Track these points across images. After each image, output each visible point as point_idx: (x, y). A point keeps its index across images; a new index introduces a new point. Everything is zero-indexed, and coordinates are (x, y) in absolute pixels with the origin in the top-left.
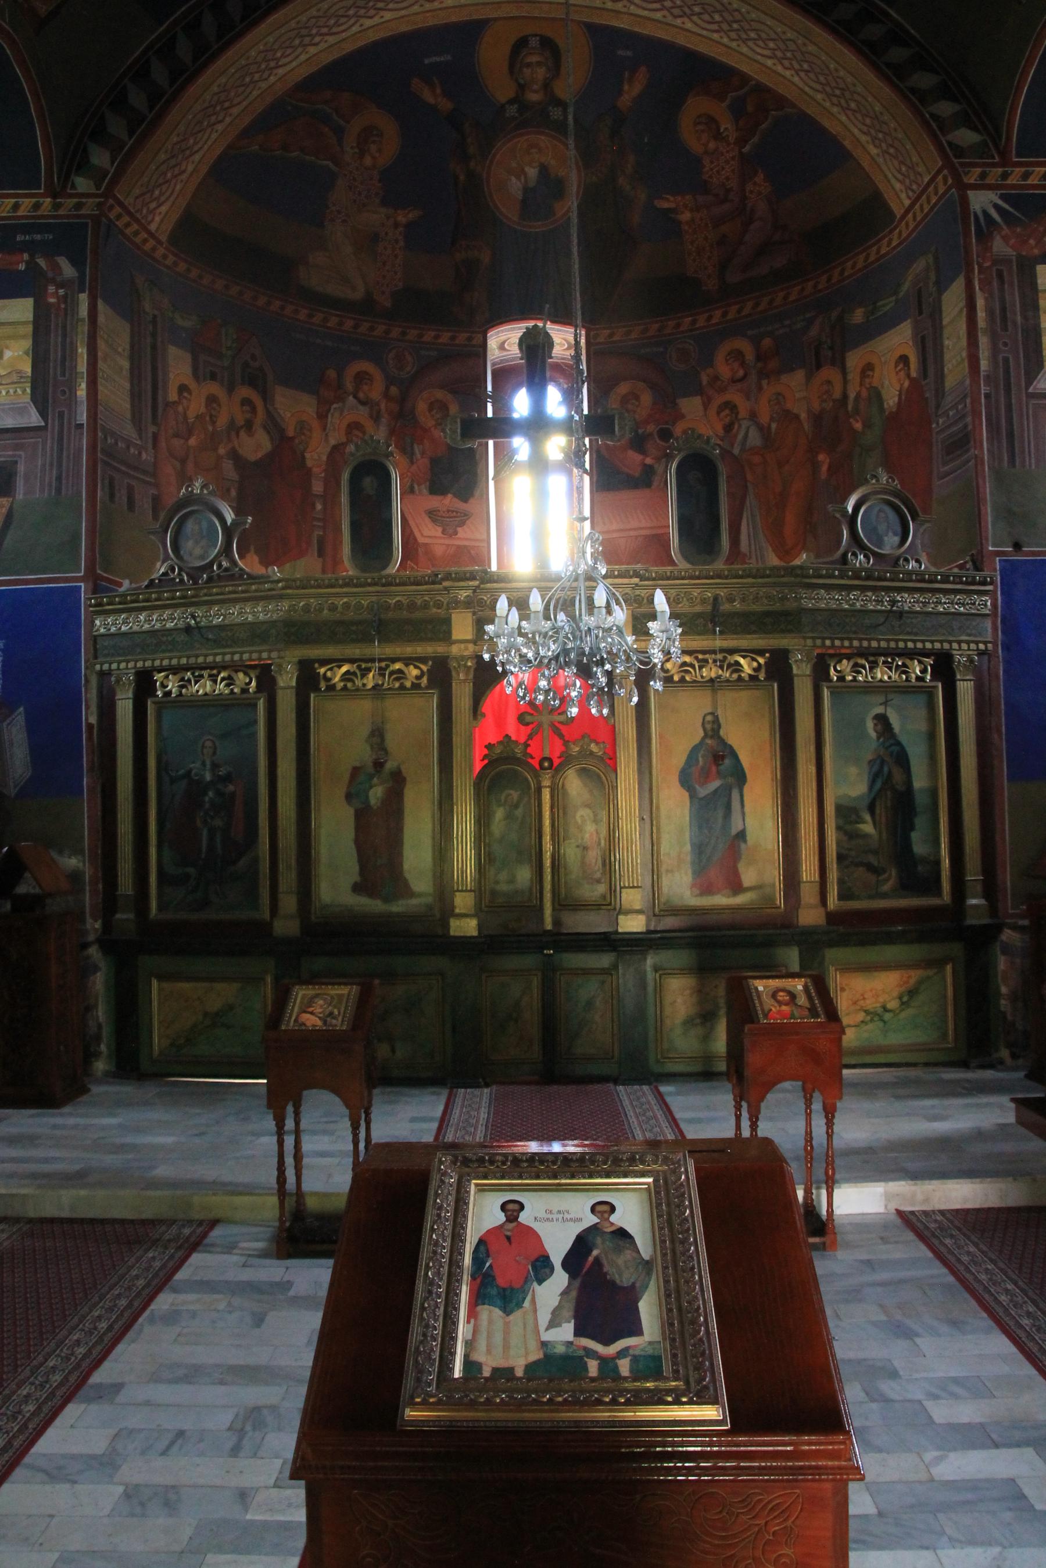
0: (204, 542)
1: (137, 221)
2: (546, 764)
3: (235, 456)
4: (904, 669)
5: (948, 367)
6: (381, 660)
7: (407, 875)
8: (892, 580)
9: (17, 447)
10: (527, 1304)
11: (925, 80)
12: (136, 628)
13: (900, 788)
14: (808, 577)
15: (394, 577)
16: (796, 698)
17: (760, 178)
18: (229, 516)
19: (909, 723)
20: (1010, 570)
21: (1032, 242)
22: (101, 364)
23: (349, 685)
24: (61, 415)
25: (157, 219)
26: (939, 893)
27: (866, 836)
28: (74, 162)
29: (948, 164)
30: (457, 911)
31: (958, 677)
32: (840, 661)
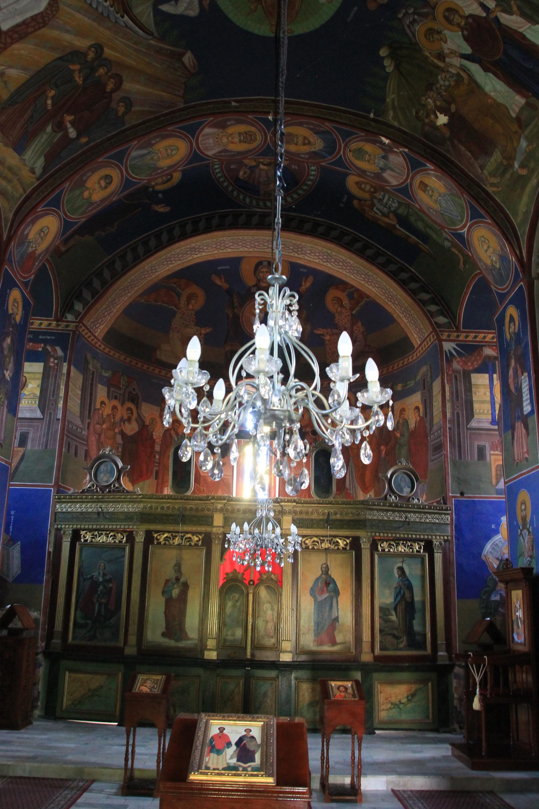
0: (108, 475)
1: (91, 332)
2: (251, 583)
3: (122, 433)
4: (411, 547)
5: (435, 414)
6: (182, 532)
7: (187, 630)
8: (406, 508)
9: (29, 426)
10: (224, 753)
11: (425, 296)
12: (74, 510)
13: (409, 600)
14: (369, 505)
15: (190, 497)
16: (363, 557)
17: (360, 324)
18: (120, 465)
19: (413, 571)
20: (458, 504)
21: (469, 364)
22: (70, 393)
23: (167, 542)
24: (51, 414)
25: (99, 331)
26: (425, 649)
27: (392, 621)
28: (67, 307)
29: (434, 330)
30: (208, 647)
31: (435, 551)
32: (383, 543)
